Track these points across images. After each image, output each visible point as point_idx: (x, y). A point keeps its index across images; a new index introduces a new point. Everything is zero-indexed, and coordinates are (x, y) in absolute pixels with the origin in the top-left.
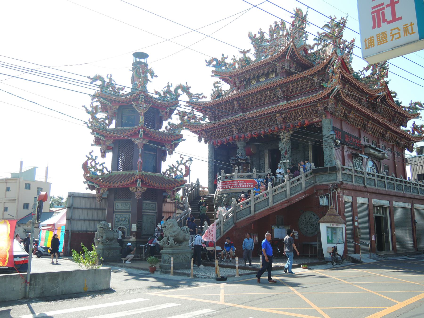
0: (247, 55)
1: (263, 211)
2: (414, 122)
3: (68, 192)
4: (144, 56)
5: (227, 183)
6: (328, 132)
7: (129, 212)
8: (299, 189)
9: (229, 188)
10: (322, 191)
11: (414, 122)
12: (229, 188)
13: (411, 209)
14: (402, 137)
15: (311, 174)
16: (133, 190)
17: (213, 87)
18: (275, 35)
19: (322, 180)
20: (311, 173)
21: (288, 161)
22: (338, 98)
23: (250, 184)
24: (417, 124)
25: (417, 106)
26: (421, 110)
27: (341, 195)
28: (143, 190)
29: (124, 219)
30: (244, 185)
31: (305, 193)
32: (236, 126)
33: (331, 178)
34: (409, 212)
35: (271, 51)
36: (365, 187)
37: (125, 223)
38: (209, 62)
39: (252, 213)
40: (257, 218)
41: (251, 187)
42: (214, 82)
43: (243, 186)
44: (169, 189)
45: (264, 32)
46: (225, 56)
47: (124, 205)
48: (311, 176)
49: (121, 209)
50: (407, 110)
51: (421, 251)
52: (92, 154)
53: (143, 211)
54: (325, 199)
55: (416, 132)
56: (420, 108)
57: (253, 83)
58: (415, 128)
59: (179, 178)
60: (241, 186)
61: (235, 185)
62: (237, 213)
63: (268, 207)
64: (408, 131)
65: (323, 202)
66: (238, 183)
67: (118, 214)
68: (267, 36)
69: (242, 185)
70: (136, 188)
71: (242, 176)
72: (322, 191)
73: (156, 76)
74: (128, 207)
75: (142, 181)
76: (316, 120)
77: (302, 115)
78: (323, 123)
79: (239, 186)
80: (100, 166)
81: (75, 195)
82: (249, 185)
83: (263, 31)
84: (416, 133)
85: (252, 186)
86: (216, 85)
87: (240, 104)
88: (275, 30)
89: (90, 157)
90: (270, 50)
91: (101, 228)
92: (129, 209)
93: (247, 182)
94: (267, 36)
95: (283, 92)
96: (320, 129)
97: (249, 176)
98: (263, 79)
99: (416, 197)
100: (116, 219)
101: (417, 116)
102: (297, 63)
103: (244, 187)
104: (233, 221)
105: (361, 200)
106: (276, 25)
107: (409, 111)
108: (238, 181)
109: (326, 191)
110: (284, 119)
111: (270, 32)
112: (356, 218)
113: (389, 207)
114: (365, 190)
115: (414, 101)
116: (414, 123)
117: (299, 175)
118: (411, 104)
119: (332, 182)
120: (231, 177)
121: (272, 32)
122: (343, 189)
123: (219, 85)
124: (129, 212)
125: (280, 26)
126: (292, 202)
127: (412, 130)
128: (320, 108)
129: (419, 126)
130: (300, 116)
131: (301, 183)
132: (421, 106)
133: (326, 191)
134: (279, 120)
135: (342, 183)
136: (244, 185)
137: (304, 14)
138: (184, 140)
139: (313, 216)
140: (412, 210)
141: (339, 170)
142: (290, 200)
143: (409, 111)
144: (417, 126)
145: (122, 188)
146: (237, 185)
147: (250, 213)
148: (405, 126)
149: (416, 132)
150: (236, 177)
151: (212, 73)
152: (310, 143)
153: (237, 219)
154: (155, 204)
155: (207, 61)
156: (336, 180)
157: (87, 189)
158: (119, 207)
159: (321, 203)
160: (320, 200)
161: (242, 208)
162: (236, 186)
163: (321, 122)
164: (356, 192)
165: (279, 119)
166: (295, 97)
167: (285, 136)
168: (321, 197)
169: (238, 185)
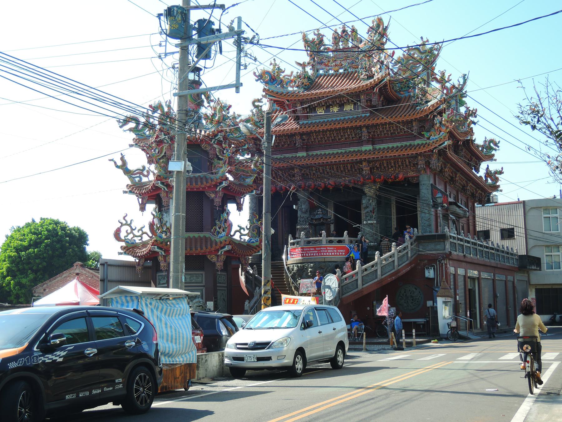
1: (371, 285)
2: (488, 166)
5: (311, 249)
6: (425, 192)
8: (406, 259)
9: (313, 255)
10: (426, 261)
11: (488, 166)
12: (311, 256)
13: (493, 280)
14: (470, 181)
15: (415, 242)
16: (212, 258)
17: (253, 108)
18: (341, 43)
20: (415, 241)
21: (375, 222)
22: (442, 153)
23: (341, 251)
24: (490, 169)
25: (492, 145)
26: (496, 150)
27: (448, 266)
30: (334, 253)
31: (410, 264)
32: (301, 170)
33: (438, 247)
34: (491, 281)
35: (336, 65)
36: (464, 256)
38: (259, 76)
39: (360, 287)
40: (365, 293)
41: (342, 255)
42: (252, 100)
43: (333, 254)
44: (210, 253)
45: (323, 36)
47: (195, 278)
48: (415, 244)
50: (480, 149)
51: (501, 330)
52: (126, 218)
53: (218, 285)
54: (432, 271)
55: (489, 179)
56: (494, 147)
58: (489, 174)
59: (253, 242)
60: (330, 254)
61: (324, 253)
62: (342, 287)
63: (376, 280)
64: (481, 177)
65: (430, 273)
66: (327, 250)
68: (328, 41)
69: (332, 253)
70: (218, 256)
71: (331, 242)
72: (426, 261)
74: (200, 280)
76: (411, 174)
77: (395, 167)
78: (421, 179)
79: (328, 254)
80: (138, 231)
81: (109, 263)
84: (490, 181)
85: (344, 254)
86: (256, 104)
87: (304, 140)
89: (124, 222)
90: (334, 64)
91: (199, 306)
92: (202, 283)
93: (338, 248)
94: (328, 41)
95: (369, 133)
96: (417, 185)
97: (340, 242)
98: (336, 109)
99: (499, 266)
101: (491, 158)
102: (384, 98)
103: (335, 255)
104: (339, 296)
105: (461, 271)
107: (482, 150)
108: (326, 247)
109: (432, 261)
110: (371, 168)
111: (335, 38)
112: (458, 292)
113: (478, 278)
114: (464, 260)
115: (488, 138)
116: (488, 168)
117: (404, 243)
118: (485, 141)
119: (438, 252)
121: (336, 39)
122: (450, 259)
123: (260, 104)
125: (350, 33)
126: (400, 274)
127: (485, 176)
128: (421, 163)
129: (493, 172)
130: (392, 167)
131: (407, 253)
132: (496, 144)
133: (432, 261)
134: (366, 170)
135: (450, 253)
136: (334, 253)
137: (385, 25)
139: (414, 290)
140: (494, 280)
141: (448, 239)
142: (398, 271)
143: (482, 150)
144: (491, 171)
147: (357, 287)
148: (477, 170)
149: (489, 179)
151: (263, 91)
152: (393, 198)
153: (343, 295)
154: (202, 274)
155: (257, 74)
156: (445, 249)
157: (120, 254)
159: (427, 274)
160: (426, 272)
161: (348, 281)
162: (325, 254)
163: (418, 177)
164: (459, 262)
165: (366, 170)
166: (382, 142)
167: (370, 191)
168: (428, 268)
169: (337, 252)
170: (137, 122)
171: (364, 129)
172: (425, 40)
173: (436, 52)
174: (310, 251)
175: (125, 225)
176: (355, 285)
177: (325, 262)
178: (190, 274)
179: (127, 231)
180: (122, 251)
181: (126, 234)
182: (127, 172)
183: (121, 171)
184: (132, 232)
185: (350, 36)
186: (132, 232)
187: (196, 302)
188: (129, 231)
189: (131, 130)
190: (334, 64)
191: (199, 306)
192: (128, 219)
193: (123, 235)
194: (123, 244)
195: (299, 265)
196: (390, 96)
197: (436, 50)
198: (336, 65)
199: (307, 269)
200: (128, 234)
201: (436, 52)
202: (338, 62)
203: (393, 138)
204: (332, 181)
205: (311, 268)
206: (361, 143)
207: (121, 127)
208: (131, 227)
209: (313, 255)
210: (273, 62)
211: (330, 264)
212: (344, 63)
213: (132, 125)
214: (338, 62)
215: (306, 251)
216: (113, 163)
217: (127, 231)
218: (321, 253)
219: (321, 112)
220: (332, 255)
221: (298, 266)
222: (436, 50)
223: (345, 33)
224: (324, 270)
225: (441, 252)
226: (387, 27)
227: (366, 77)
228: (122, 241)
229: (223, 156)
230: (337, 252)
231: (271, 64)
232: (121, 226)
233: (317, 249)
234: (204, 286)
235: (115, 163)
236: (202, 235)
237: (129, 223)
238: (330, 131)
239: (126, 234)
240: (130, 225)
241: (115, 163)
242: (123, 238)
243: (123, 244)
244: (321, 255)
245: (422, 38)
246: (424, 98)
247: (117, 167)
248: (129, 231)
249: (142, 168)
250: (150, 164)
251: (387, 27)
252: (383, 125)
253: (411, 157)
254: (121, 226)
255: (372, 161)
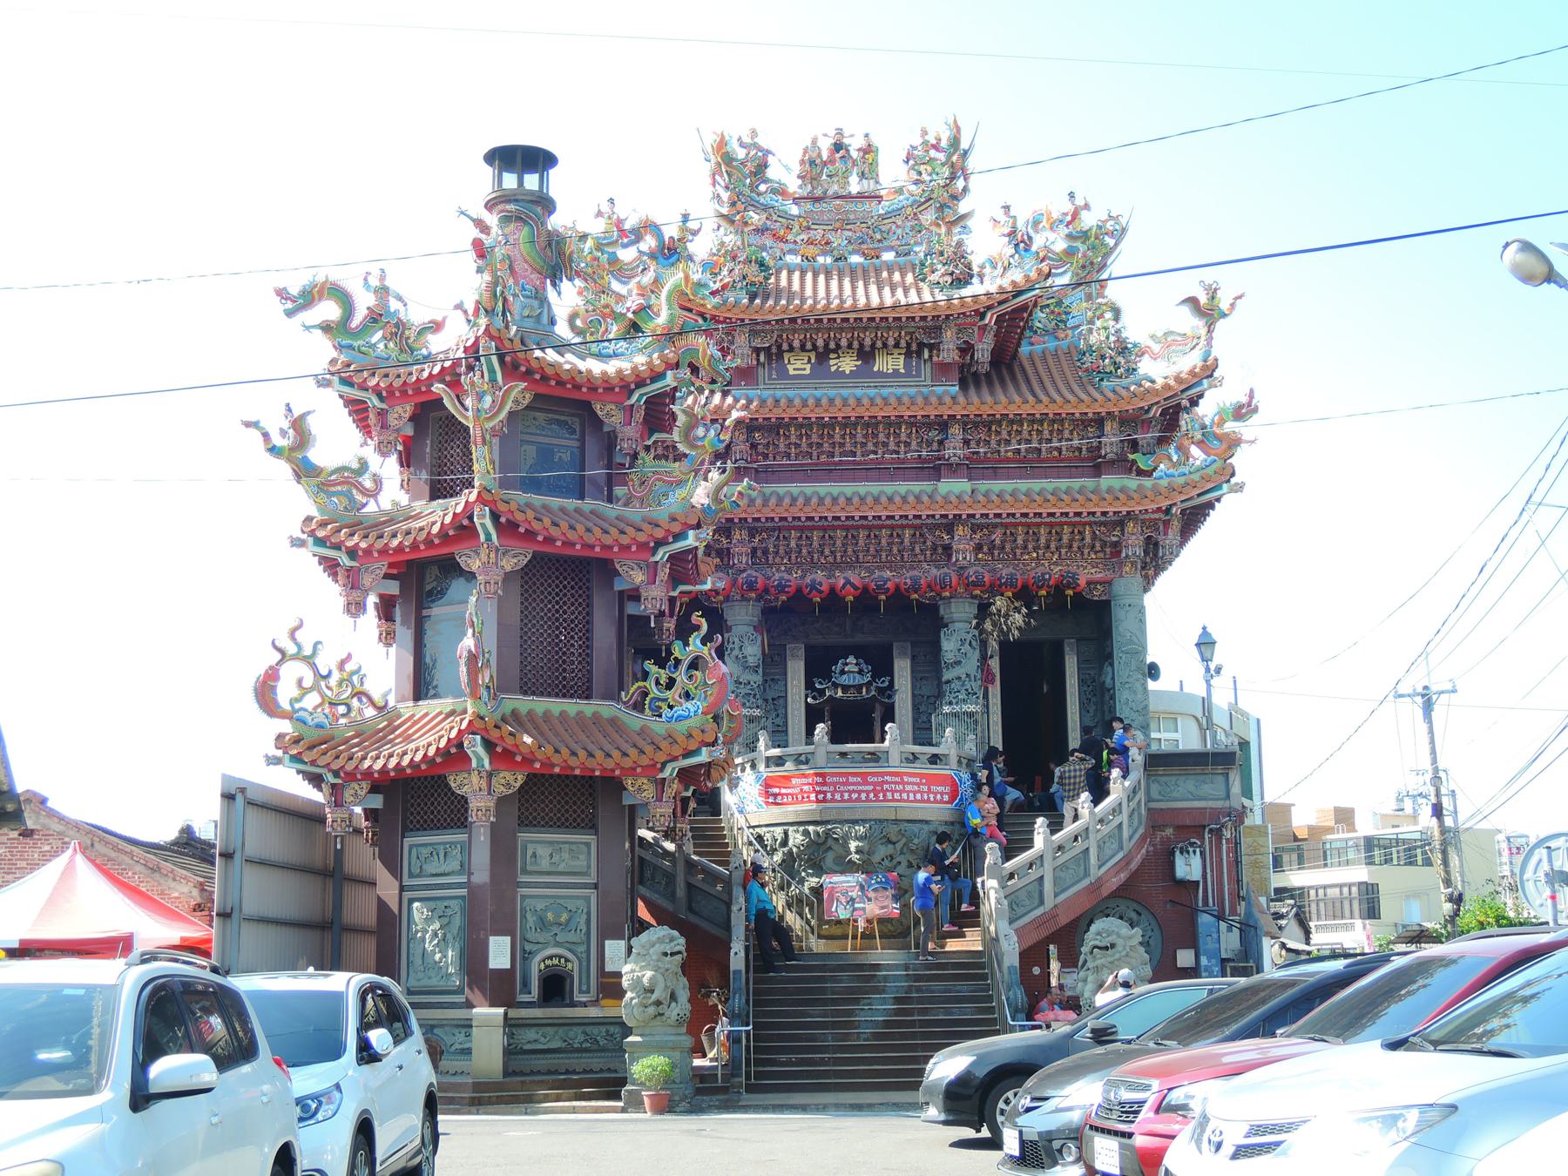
0: (975, 280)
3: (224, 776)
4: (535, 159)
7: (585, 886)
9: (858, 800)
10: (1169, 831)
19: (1175, 794)
23: (940, 789)
28: (508, 785)
29: (564, 917)
30: (922, 793)
33: (1207, 789)
37: (572, 937)
39: (1049, 902)
41: (942, 802)
43: (855, 796)
45: (768, 152)
46: (692, 225)
47: (566, 856)
49: (549, 873)
52: (298, 635)
54: (1196, 861)
57: (798, 365)
61: (893, 792)
63: (1086, 882)
67: (533, 897)
69: (915, 793)
73: (1251, 396)
74: (580, 863)
75: (489, 745)
76: (1086, 573)
79: (905, 796)
81: (250, 794)
82: (935, 794)
83: (762, 141)
85: (946, 798)
88: (832, 161)
89: (291, 649)
90: (804, 236)
93: (932, 780)
94: (785, 171)
97: (934, 759)
98: (848, 364)
100: (531, 919)
103: (922, 801)
106: (838, 146)
120: (874, 757)
121: (812, 167)
124: (585, 886)
125: (854, 154)
126: (1134, 866)
130: (1035, 549)
136: (922, 793)
137: (964, 145)
138: (1239, 488)
145: (559, 776)
146: (901, 792)
147: (1042, 903)
150: (895, 758)
154: (588, 845)
156: (1228, 797)
157: (273, 761)
158: (545, 864)
162: (897, 796)
169: (929, 791)
170: (345, 300)
171: (955, 430)
172: (1080, 202)
173: (1111, 242)
174: (847, 783)
175: (294, 657)
176: (1036, 895)
177: (896, 821)
178: (551, 843)
179: (300, 681)
180: (279, 753)
181: (296, 693)
182: (305, 471)
183: (284, 469)
184: (315, 687)
185: (854, 163)
186: (315, 687)
187: (660, 940)
188: (308, 683)
189: (326, 328)
190: (804, 236)
191: (672, 954)
192: (306, 639)
193: (285, 693)
194: (286, 726)
195: (811, 828)
196: (1001, 343)
197: (1111, 234)
198: (810, 242)
199: (846, 839)
200: (305, 691)
201: (1111, 242)
202: (817, 234)
203: (1030, 465)
204: (856, 577)
205: (857, 838)
206: (935, 469)
207: (290, 314)
208: (314, 667)
209: (858, 800)
210: (605, 208)
211: (915, 828)
212: (838, 240)
213: (329, 310)
214: (817, 234)
215: (834, 784)
216: (256, 435)
217: (300, 681)
218: (885, 792)
219: (798, 365)
220: (916, 801)
221: (806, 833)
222: (1111, 234)
223: (842, 153)
224: (899, 846)
225: (1219, 804)
226: (966, 152)
227: (949, 279)
228: (283, 715)
229: (693, 447)
230: (929, 791)
231: (599, 214)
232: (280, 663)
233: (871, 779)
234: (596, 886)
235: (266, 436)
236: (589, 707)
237: (308, 651)
238: (844, 426)
239: (296, 693)
240: (309, 661)
241: (266, 436)
242: (286, 705)
243: (286, 726)
244: (885, 800)
245: (1072, 195)
246: (1120, 359)
247: (273, 450)
248: (308, 683)
249: (355, 465)
250: (384, 454)
251: (966, 152)
252: (1012, 422)
253: (1104, 524)
254: (280, 663)
255: (980, 527)
